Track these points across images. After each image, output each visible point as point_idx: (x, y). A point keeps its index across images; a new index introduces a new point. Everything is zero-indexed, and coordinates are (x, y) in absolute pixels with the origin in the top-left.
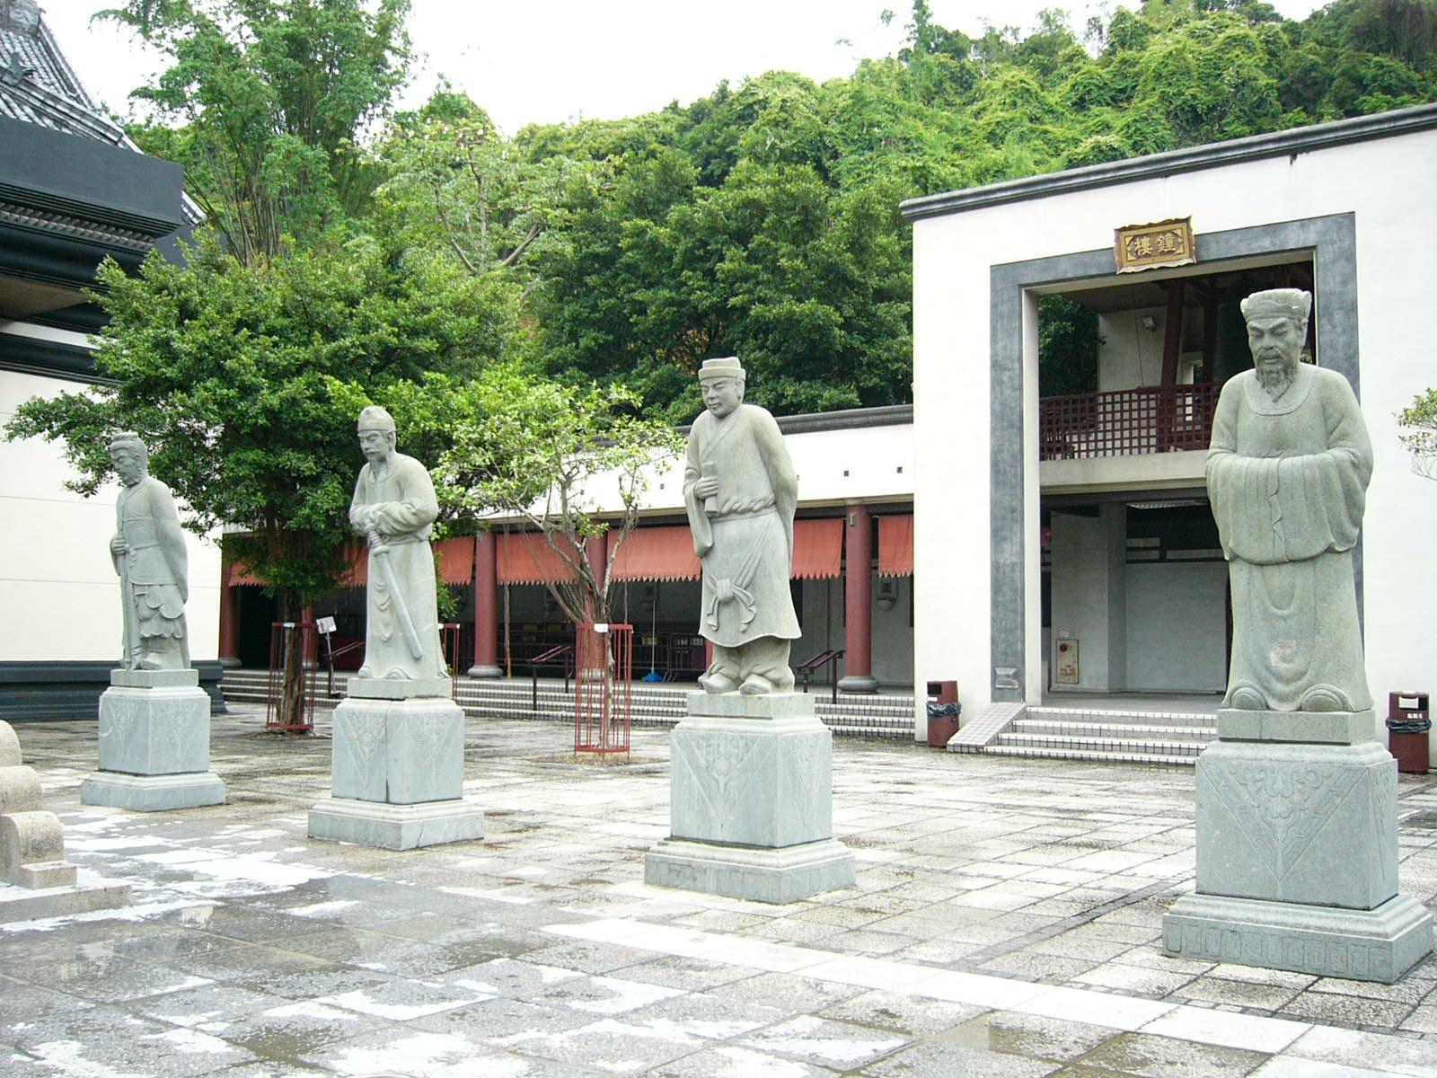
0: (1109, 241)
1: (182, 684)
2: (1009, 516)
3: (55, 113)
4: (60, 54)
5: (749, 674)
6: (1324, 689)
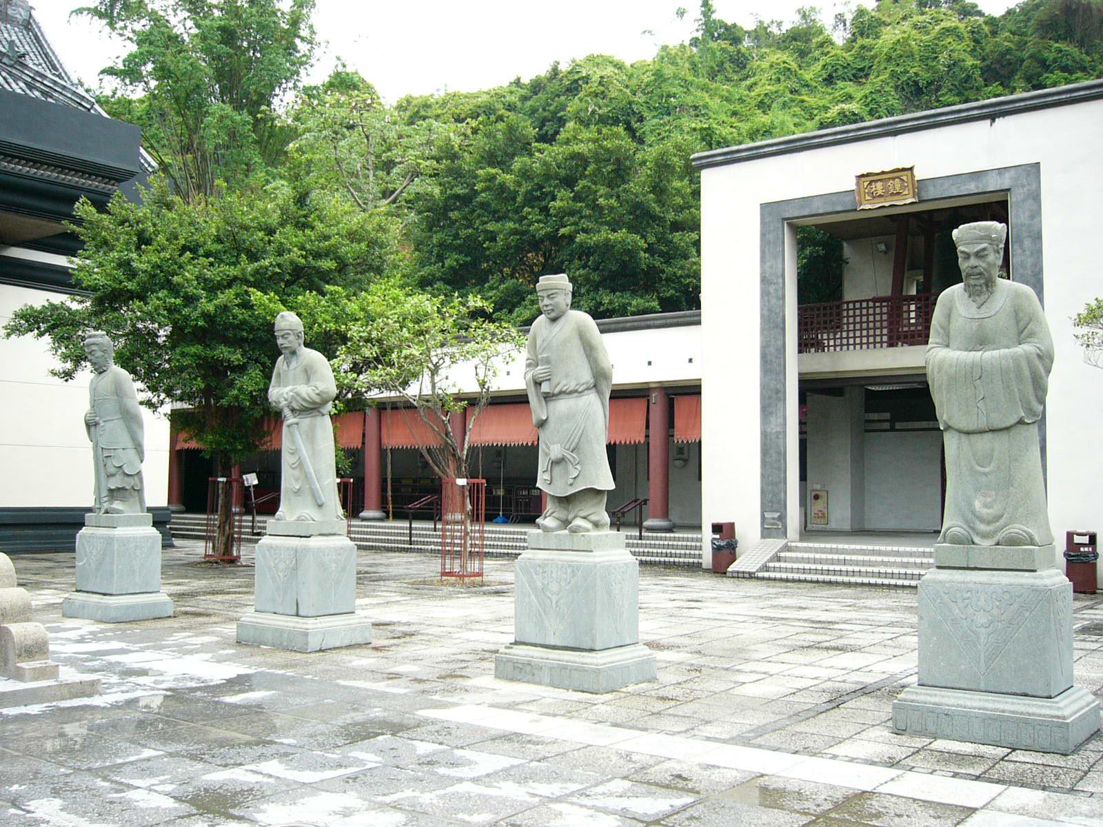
0: (851, 185)
1: (140, 525)
2: (774, 396)
3: (42, 87)
4: (46, 41)
5: (575, 517)
6: (1016, 529)
